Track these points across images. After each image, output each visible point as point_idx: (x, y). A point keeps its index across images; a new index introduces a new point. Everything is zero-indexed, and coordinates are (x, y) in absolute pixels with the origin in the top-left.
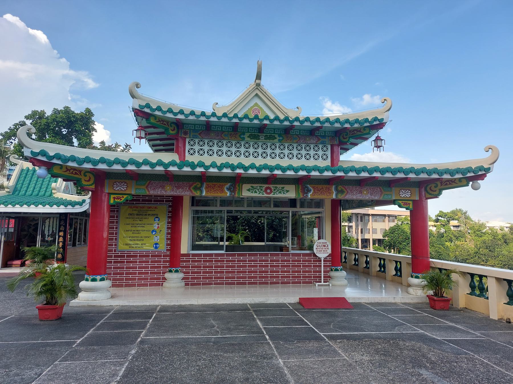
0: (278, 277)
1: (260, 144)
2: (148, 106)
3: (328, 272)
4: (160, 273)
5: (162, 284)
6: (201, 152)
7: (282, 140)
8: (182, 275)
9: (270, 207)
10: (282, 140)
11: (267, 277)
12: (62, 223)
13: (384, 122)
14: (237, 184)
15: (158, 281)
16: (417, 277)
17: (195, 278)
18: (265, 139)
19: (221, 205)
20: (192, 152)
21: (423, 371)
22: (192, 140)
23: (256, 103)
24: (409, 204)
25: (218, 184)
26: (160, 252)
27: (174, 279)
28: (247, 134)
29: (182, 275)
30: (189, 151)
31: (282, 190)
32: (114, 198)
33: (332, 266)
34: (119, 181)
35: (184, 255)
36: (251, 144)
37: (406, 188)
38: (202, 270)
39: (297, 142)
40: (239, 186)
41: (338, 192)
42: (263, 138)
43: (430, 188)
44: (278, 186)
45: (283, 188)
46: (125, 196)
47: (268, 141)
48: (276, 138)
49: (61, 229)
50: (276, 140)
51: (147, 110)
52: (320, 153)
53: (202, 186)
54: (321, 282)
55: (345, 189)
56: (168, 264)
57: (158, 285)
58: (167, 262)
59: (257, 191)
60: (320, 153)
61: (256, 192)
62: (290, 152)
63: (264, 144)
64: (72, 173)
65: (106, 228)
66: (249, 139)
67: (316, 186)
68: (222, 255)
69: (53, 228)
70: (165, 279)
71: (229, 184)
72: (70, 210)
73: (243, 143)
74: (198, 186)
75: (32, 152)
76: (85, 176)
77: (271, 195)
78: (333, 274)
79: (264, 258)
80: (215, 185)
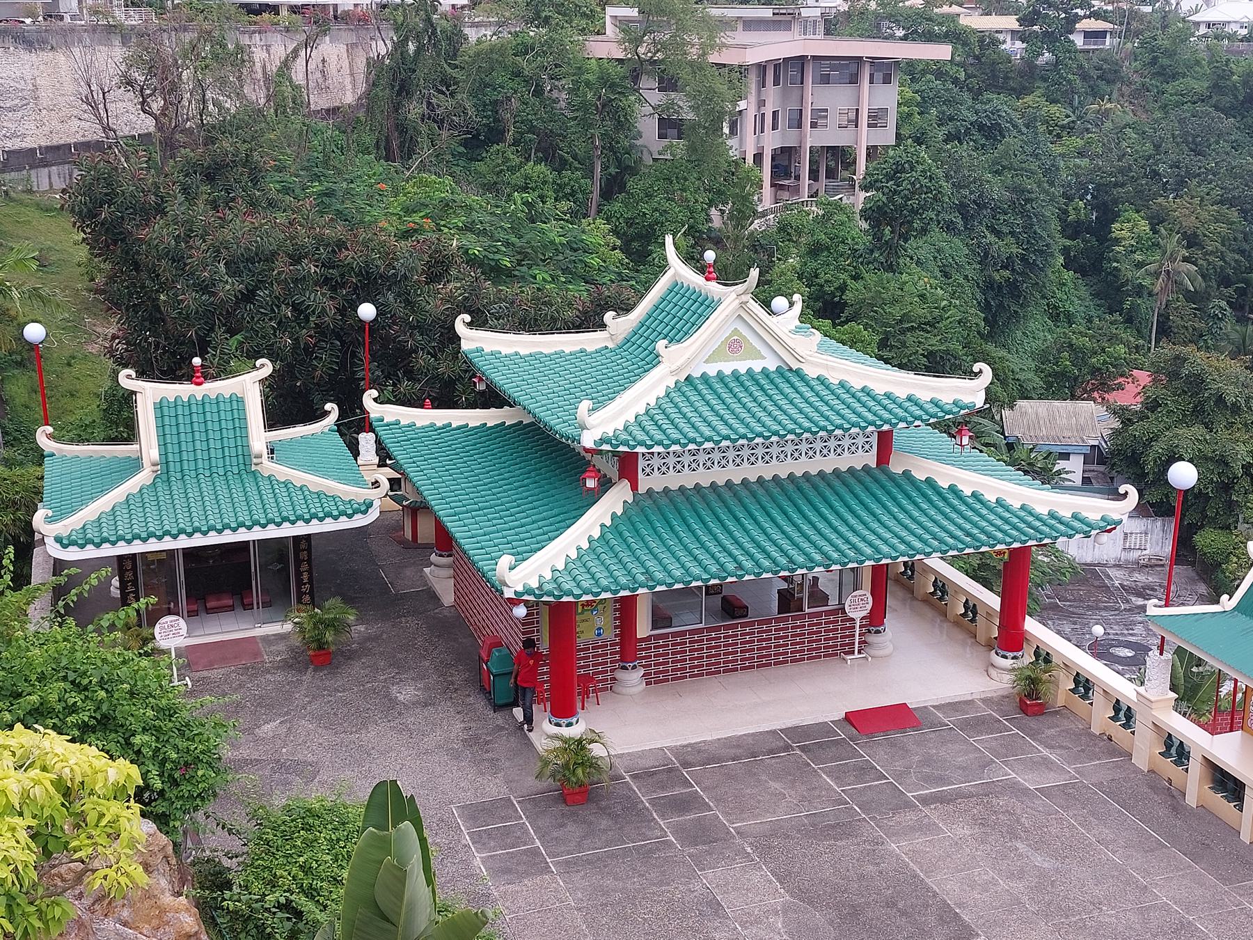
16: (1005, 657)
17: (661, 672)
20: (648, 470)
21: (1019, 845)
26: (605, 640)
35: (643, 640)
54: (853, 653)
58: (616, 653)
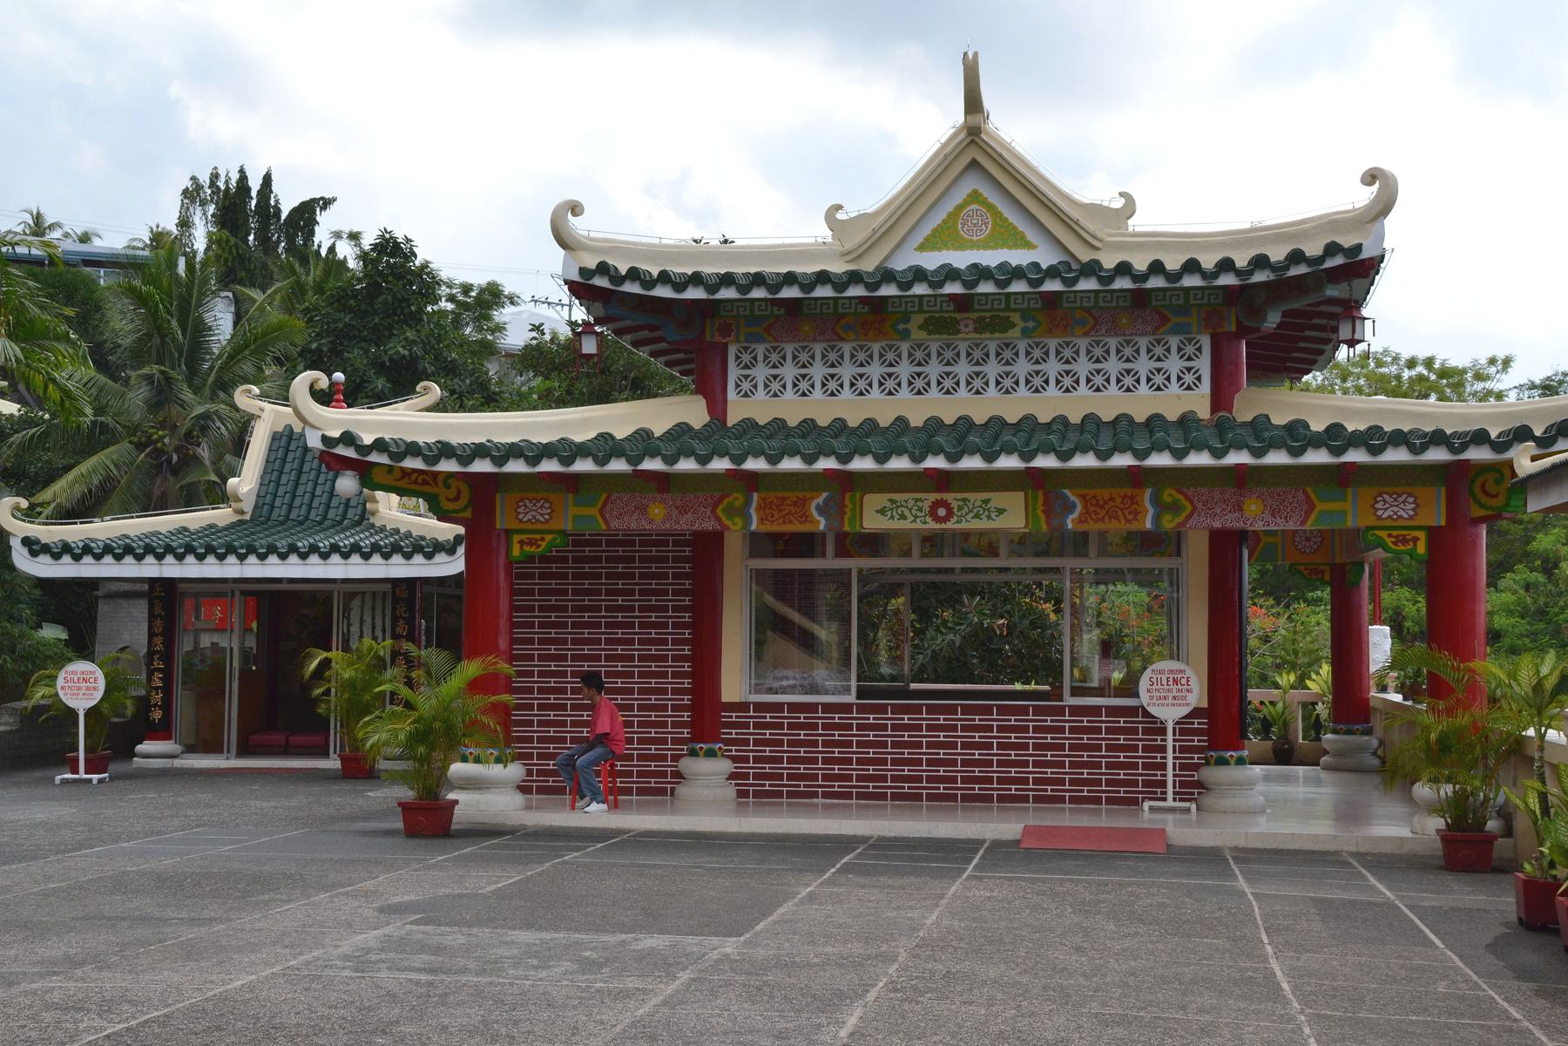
0: (1025, 781)
1: (963, 348)
2: (603, 268)
3: (1196, 767)
4: (664, 758)
5: (673, 790)
6: (775, 385)
7: (1035, 328)
8: (726, 766)
9: (860, 571)
10: (1035, 328)
11: (990, 780)
12: (401, 610)
13: (1365, 255)
14: (848, 495)
15: (661, 786)
18: (976, 331)
19: (842, 552)
20: (746, 386)
22: (746, 349)
23: (975, 191)
24: (1415, 540)
25: (793, 495)
27: (709, 774)
28: (917, 320)
29: (726, 766)
30: (738, 386)
31: (985, 509)
32: (522, 543)
33: (1210, 748)
34: (531, 495)
36: (934, 348)
37: (1399, 490)
38: (785, 751)
39: (1086, 334)
40: (853, 501)
41: (1161, 508)
42: (971, 327)
43: (1483, 486)
44: (972, 496)
45: (986, 501)
46: (549, 537)
47: (988, 335)
48: (1013, 325)
49: (399, 630)
50: (1014, 333)
51: (601, 282)
52: (1174, 365)
53: (748, 503)
54: (1165, 799)
55: (1188, 498)
56: (686, 733)
57: (662, 792)
59: (907, 512)
60: (1174, 365)
61: (903, 517)
62: (1067, 367)
63: (977, 346)
64: (416, 482)
65: (503, 624)
66: (922, 335)
67: (1091, 492)
68: (846, 708)
69: (374, 628)
70: (678, 775)
71: (825, 495)
72: (418, 568)
73: (905, 347)
74: (738, 503)
75: (325, 439)
76: (448, 486)
77: (949, 525)
78: (1213, 774)
79: (977, 720)
80: (784, 499)
